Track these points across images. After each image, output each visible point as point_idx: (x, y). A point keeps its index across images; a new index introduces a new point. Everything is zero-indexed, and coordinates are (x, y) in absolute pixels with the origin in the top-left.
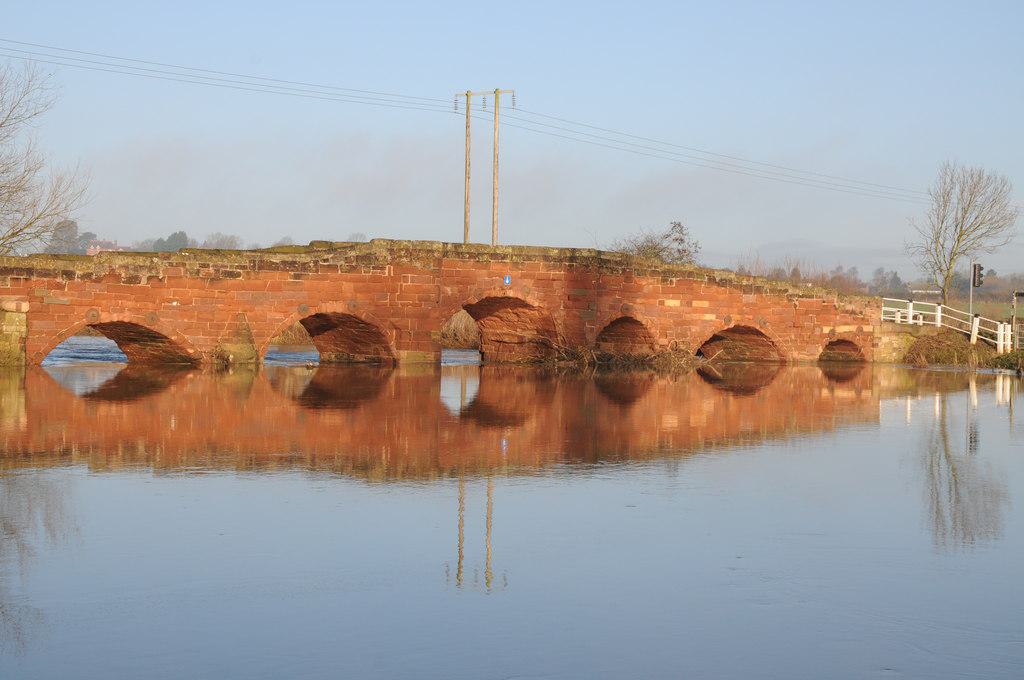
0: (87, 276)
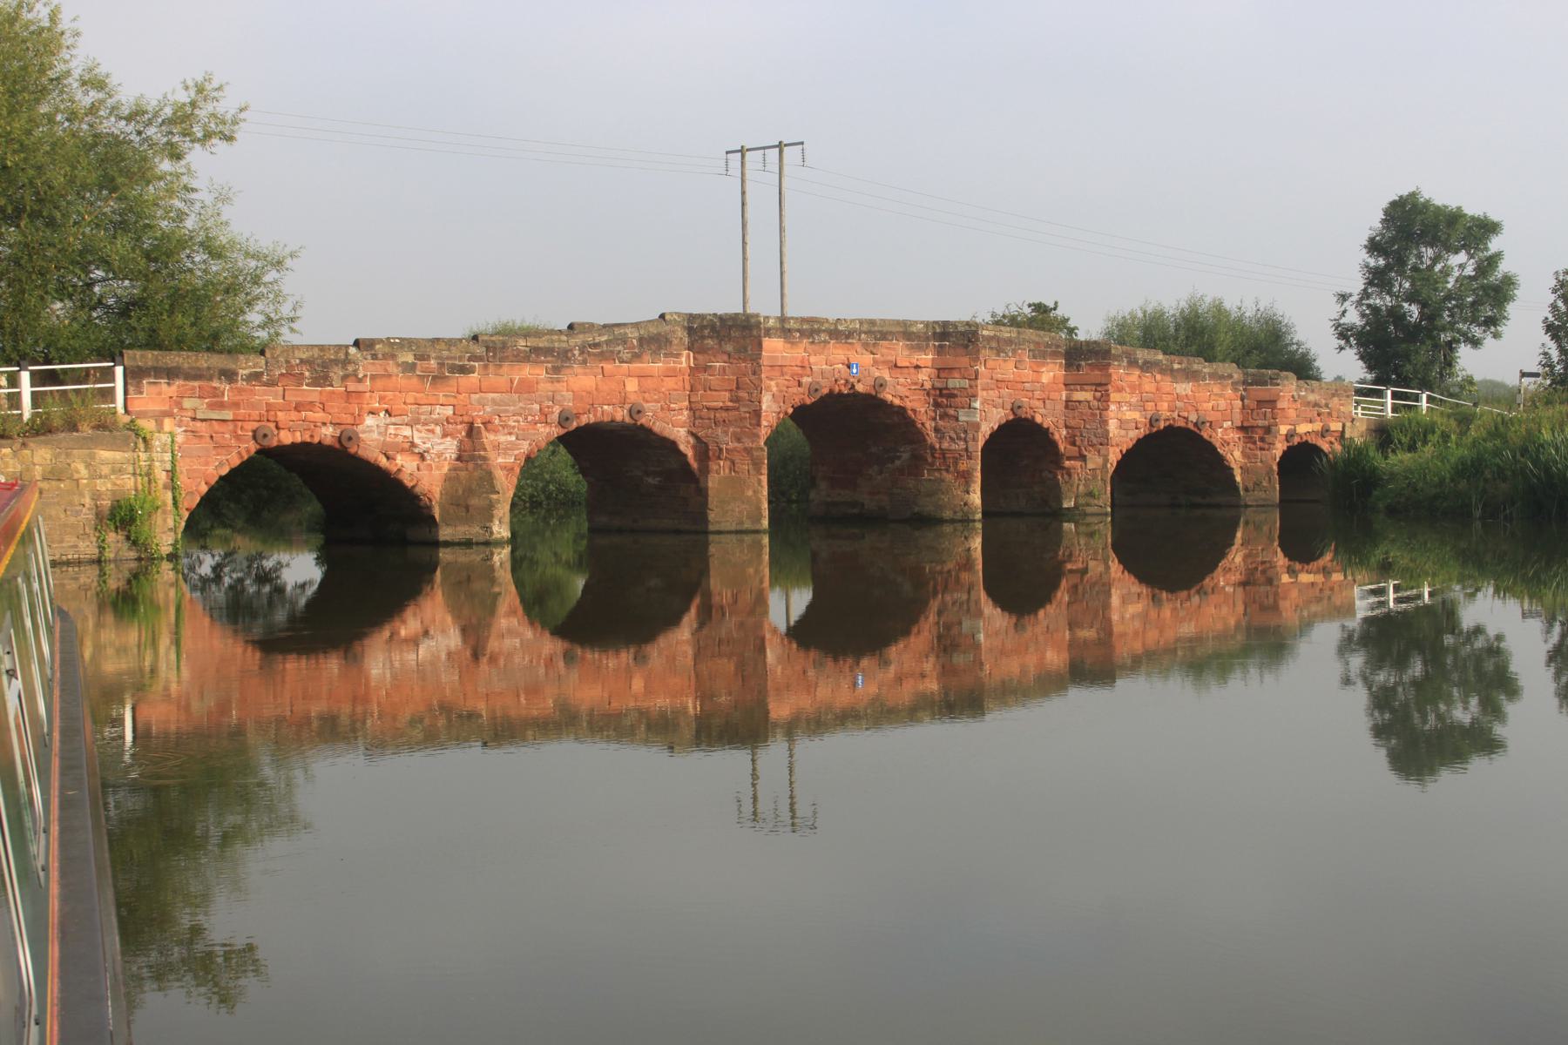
0: (256, 376)
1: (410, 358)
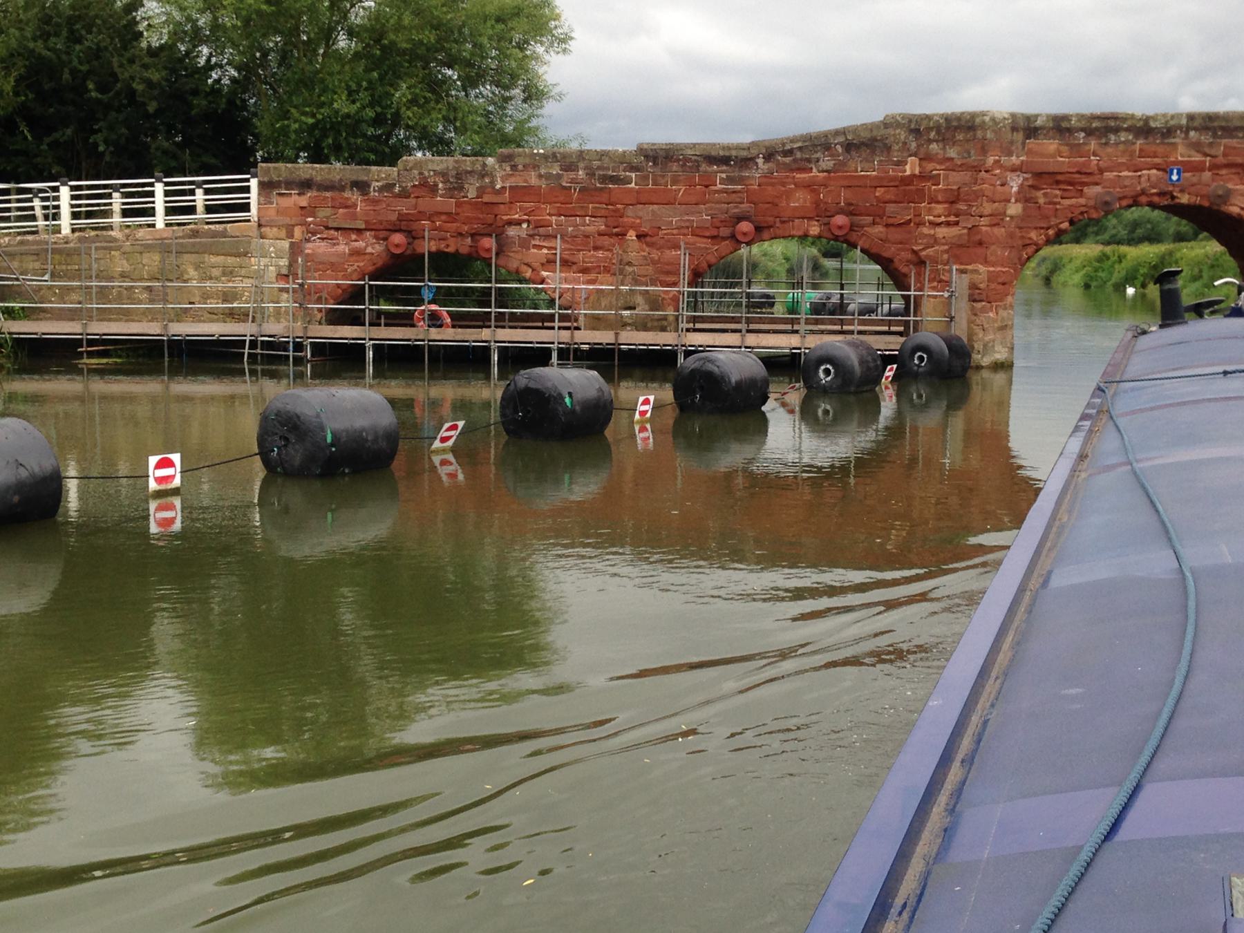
1: (555, 170)
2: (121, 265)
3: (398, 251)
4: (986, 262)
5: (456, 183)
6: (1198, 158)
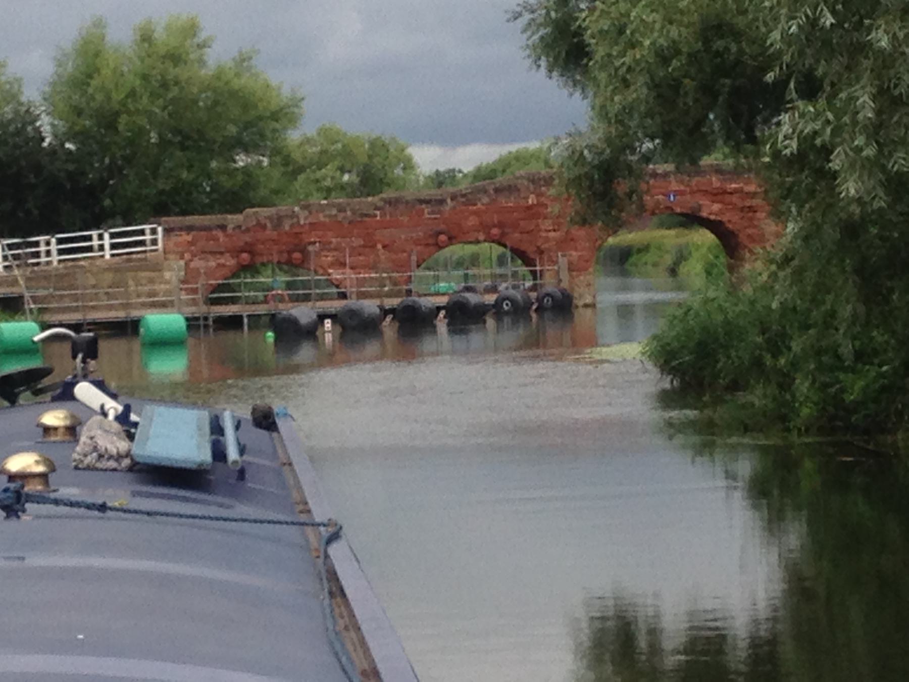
1: (334, 212)
2: (92, 281)
3: (245, 263)
4: (576, 249)
5: (278, 221)
6: (682, 188)
